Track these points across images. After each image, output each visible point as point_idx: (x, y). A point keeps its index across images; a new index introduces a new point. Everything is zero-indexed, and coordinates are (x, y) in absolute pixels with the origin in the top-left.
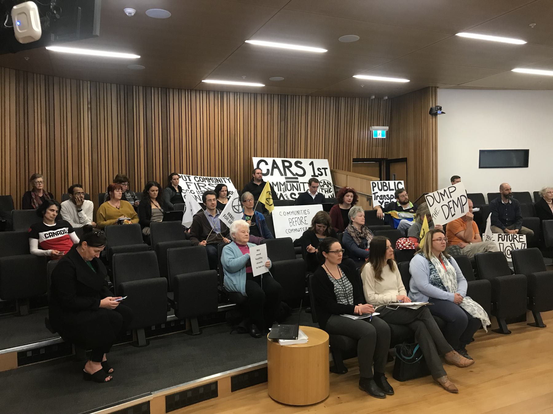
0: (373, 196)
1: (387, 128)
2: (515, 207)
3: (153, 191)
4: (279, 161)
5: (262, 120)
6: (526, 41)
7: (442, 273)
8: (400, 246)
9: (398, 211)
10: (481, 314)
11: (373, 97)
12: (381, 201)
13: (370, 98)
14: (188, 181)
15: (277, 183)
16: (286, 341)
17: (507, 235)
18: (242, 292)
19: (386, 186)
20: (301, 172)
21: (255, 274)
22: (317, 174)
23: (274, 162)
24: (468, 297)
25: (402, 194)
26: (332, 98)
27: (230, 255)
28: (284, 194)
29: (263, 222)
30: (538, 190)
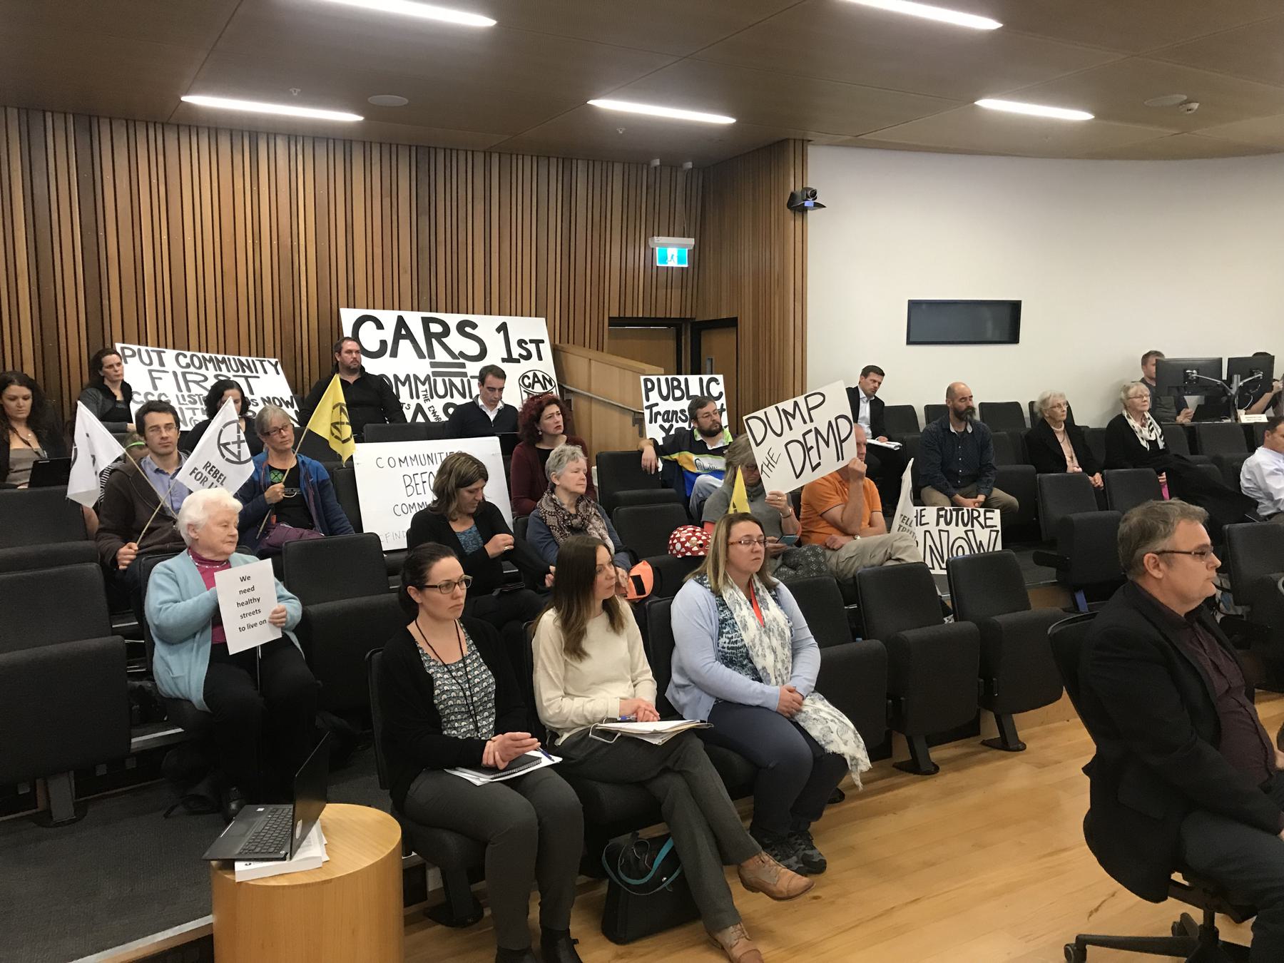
0: (647, 412)
1: (691, 241)
2: (979, 441)
3: (14, 398)
4: (414, 320)
5: (366, 209)
6: (1000, 20)
7: (750, 633)
8: (678, 546)
9: (696, 453)
10: (845, 744)
11: (657, 162)
12: (667, 425)
13: (649, 165)
14: (156, 366)
15: (408, 377)
16: (255, 865)
17: (957, 511)
18: (194, 701)
19: (679, 387)
20: (473, 349)
21: (233, 649)
22: (515, 356)
23: (401, 322)
24: (818, 696)
25: (705, 410)
26: (553, 161)
27: (170, 591)
28: (425, 406)
29: (322, 486)
30: (1036, 398)
